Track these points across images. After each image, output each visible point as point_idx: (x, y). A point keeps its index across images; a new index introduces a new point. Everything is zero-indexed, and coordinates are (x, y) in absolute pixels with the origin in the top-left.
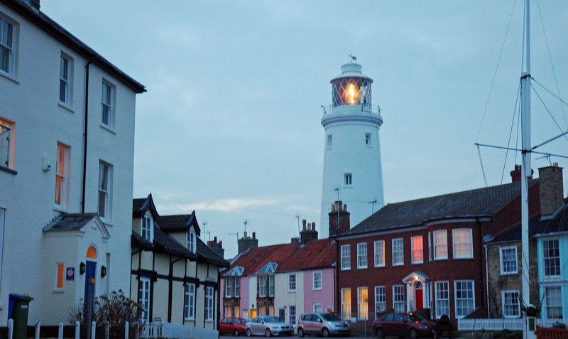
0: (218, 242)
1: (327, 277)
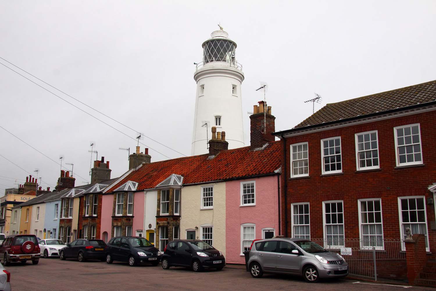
0: (105, 162)
1: (267, 190)
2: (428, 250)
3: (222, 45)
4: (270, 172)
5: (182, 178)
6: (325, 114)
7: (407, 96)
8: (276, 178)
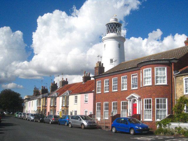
0: (55, 83)
1: (90, 97)
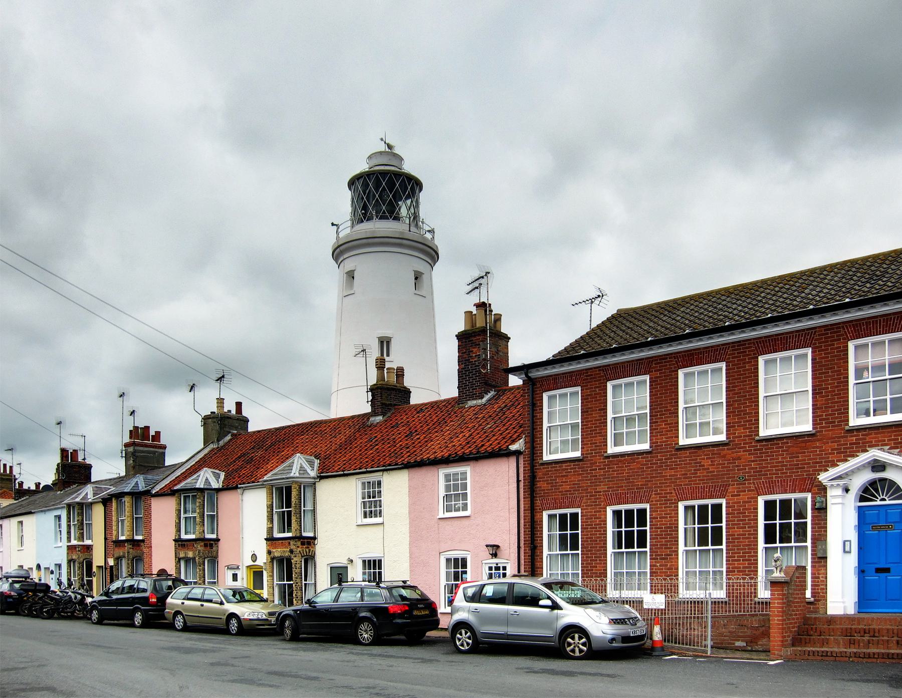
2: (808, 594)
3: (391, 185)
4: (500, 450)
5: (317, 462)
6: (615, 329)
7: (784, 293)
8: (512, 461)
